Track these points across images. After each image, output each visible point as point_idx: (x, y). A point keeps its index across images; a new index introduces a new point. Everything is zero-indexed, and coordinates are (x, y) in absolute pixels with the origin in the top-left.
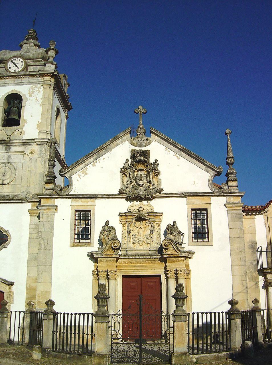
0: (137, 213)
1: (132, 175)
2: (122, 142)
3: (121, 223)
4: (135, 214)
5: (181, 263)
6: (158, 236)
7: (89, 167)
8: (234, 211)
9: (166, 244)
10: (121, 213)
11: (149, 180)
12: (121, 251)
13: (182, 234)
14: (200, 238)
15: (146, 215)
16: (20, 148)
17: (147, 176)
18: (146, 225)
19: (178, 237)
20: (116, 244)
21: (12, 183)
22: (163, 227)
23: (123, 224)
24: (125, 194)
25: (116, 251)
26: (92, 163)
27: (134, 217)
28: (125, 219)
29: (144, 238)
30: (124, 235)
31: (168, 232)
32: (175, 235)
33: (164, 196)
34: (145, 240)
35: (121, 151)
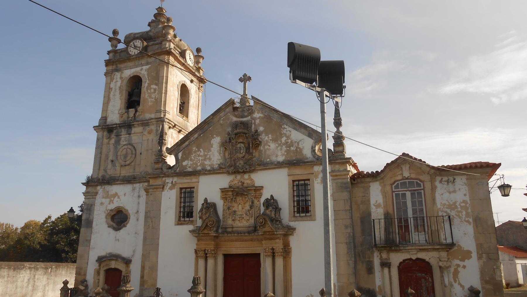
5: (277, 241)
8: (340, 181)
14: (303, 212)
21: (133, 164)
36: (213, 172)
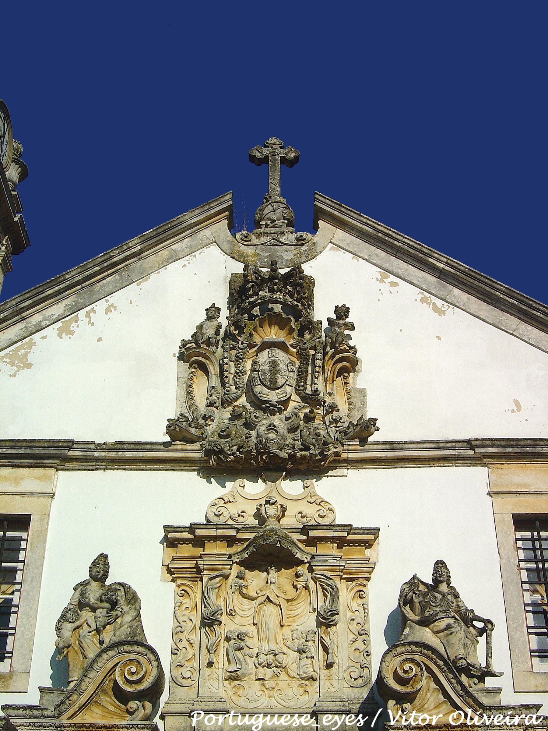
0: (250, 529)
1: (233, 370)
2: (192, 251)
3: (170, 577)
4: (241, 535)
6: (359, 644)
7: (44, 338)
9: (406, 668)
10: (176, 529)
11: (309, 391)
12: (162, 717)
13: (480, 625)
15: (295, 537)
17: (302, 374)
18: (295, 587)
19: (461, 635)
20: (134, 670)
22: (383, 597)
23: (179, 582)
24: (197, 446)
25: (133, 705)
26: (59, 324)
27: (237, 548)
28: (193, 557)
29: (285, 650)
30: (183, 636)
31: (411, 615)
32: (449, 627)
33: (383, 454)
35: (189, 280)
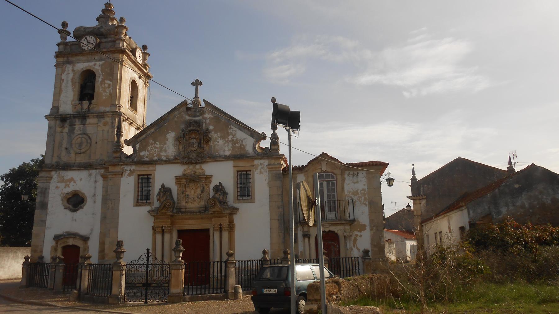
5: (224, 218)
14: (245, 196)
16: (95, 121)
22: (212, 186)
34: (194, 200)
36: (168, 162)
